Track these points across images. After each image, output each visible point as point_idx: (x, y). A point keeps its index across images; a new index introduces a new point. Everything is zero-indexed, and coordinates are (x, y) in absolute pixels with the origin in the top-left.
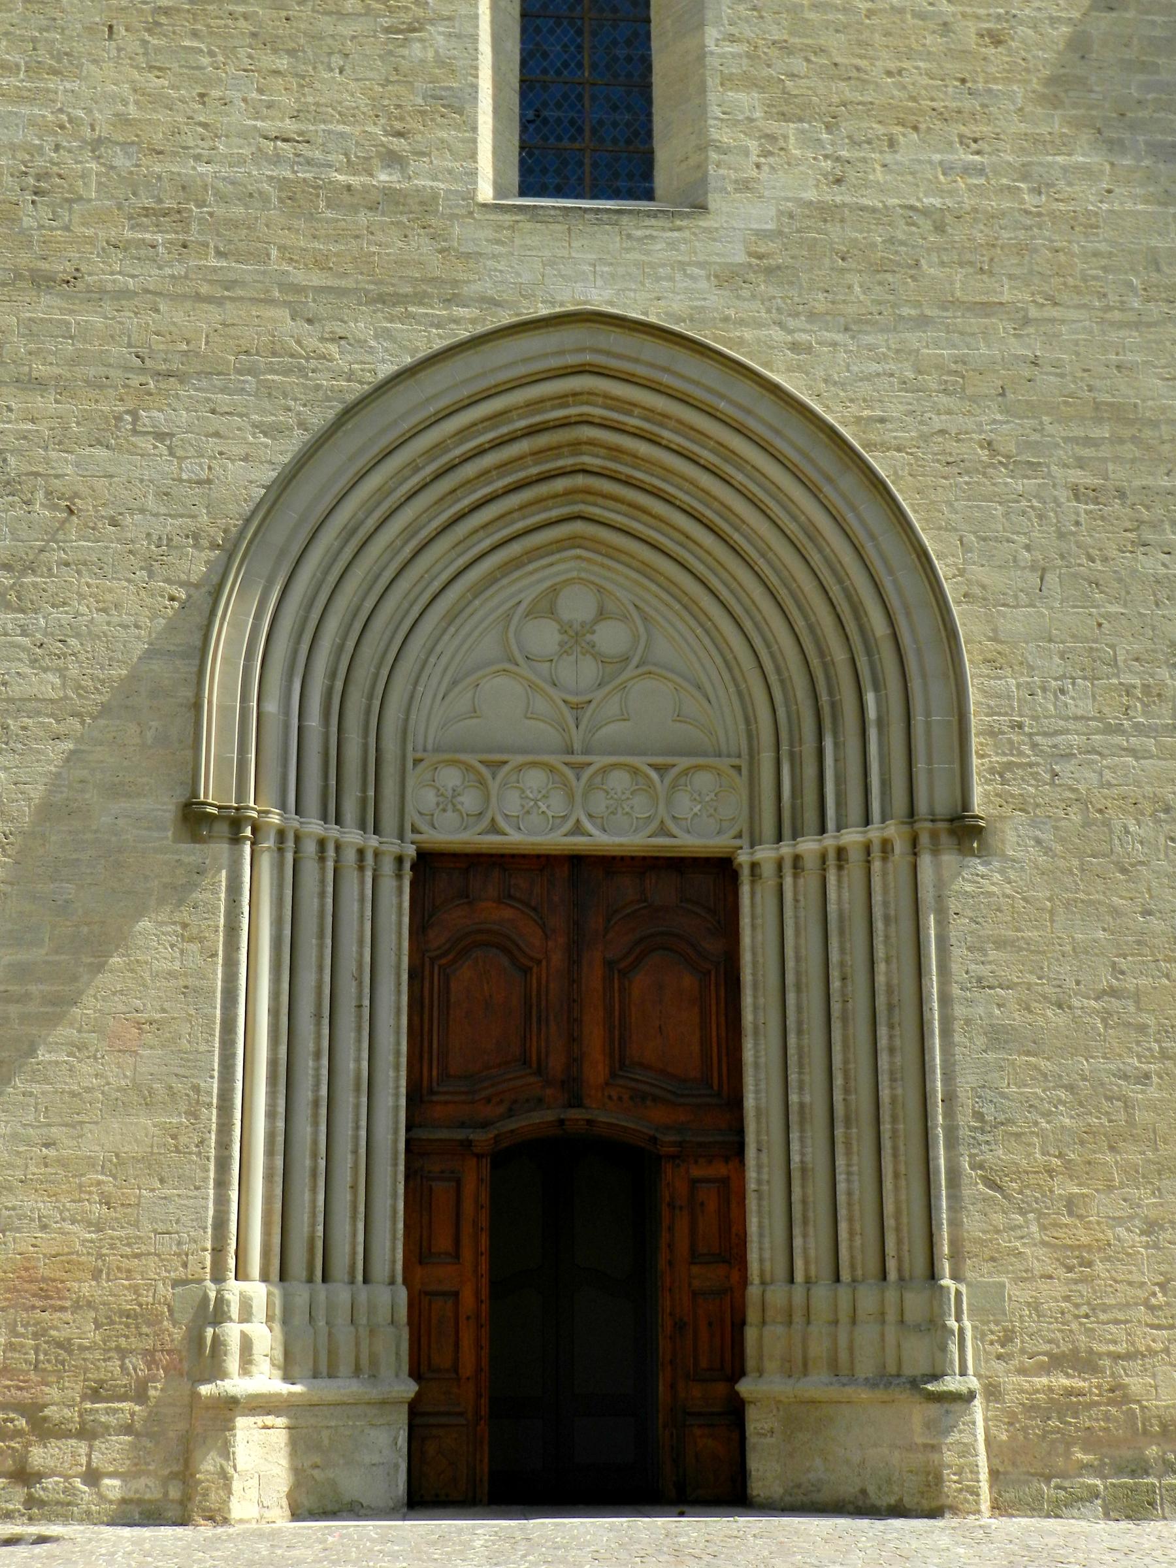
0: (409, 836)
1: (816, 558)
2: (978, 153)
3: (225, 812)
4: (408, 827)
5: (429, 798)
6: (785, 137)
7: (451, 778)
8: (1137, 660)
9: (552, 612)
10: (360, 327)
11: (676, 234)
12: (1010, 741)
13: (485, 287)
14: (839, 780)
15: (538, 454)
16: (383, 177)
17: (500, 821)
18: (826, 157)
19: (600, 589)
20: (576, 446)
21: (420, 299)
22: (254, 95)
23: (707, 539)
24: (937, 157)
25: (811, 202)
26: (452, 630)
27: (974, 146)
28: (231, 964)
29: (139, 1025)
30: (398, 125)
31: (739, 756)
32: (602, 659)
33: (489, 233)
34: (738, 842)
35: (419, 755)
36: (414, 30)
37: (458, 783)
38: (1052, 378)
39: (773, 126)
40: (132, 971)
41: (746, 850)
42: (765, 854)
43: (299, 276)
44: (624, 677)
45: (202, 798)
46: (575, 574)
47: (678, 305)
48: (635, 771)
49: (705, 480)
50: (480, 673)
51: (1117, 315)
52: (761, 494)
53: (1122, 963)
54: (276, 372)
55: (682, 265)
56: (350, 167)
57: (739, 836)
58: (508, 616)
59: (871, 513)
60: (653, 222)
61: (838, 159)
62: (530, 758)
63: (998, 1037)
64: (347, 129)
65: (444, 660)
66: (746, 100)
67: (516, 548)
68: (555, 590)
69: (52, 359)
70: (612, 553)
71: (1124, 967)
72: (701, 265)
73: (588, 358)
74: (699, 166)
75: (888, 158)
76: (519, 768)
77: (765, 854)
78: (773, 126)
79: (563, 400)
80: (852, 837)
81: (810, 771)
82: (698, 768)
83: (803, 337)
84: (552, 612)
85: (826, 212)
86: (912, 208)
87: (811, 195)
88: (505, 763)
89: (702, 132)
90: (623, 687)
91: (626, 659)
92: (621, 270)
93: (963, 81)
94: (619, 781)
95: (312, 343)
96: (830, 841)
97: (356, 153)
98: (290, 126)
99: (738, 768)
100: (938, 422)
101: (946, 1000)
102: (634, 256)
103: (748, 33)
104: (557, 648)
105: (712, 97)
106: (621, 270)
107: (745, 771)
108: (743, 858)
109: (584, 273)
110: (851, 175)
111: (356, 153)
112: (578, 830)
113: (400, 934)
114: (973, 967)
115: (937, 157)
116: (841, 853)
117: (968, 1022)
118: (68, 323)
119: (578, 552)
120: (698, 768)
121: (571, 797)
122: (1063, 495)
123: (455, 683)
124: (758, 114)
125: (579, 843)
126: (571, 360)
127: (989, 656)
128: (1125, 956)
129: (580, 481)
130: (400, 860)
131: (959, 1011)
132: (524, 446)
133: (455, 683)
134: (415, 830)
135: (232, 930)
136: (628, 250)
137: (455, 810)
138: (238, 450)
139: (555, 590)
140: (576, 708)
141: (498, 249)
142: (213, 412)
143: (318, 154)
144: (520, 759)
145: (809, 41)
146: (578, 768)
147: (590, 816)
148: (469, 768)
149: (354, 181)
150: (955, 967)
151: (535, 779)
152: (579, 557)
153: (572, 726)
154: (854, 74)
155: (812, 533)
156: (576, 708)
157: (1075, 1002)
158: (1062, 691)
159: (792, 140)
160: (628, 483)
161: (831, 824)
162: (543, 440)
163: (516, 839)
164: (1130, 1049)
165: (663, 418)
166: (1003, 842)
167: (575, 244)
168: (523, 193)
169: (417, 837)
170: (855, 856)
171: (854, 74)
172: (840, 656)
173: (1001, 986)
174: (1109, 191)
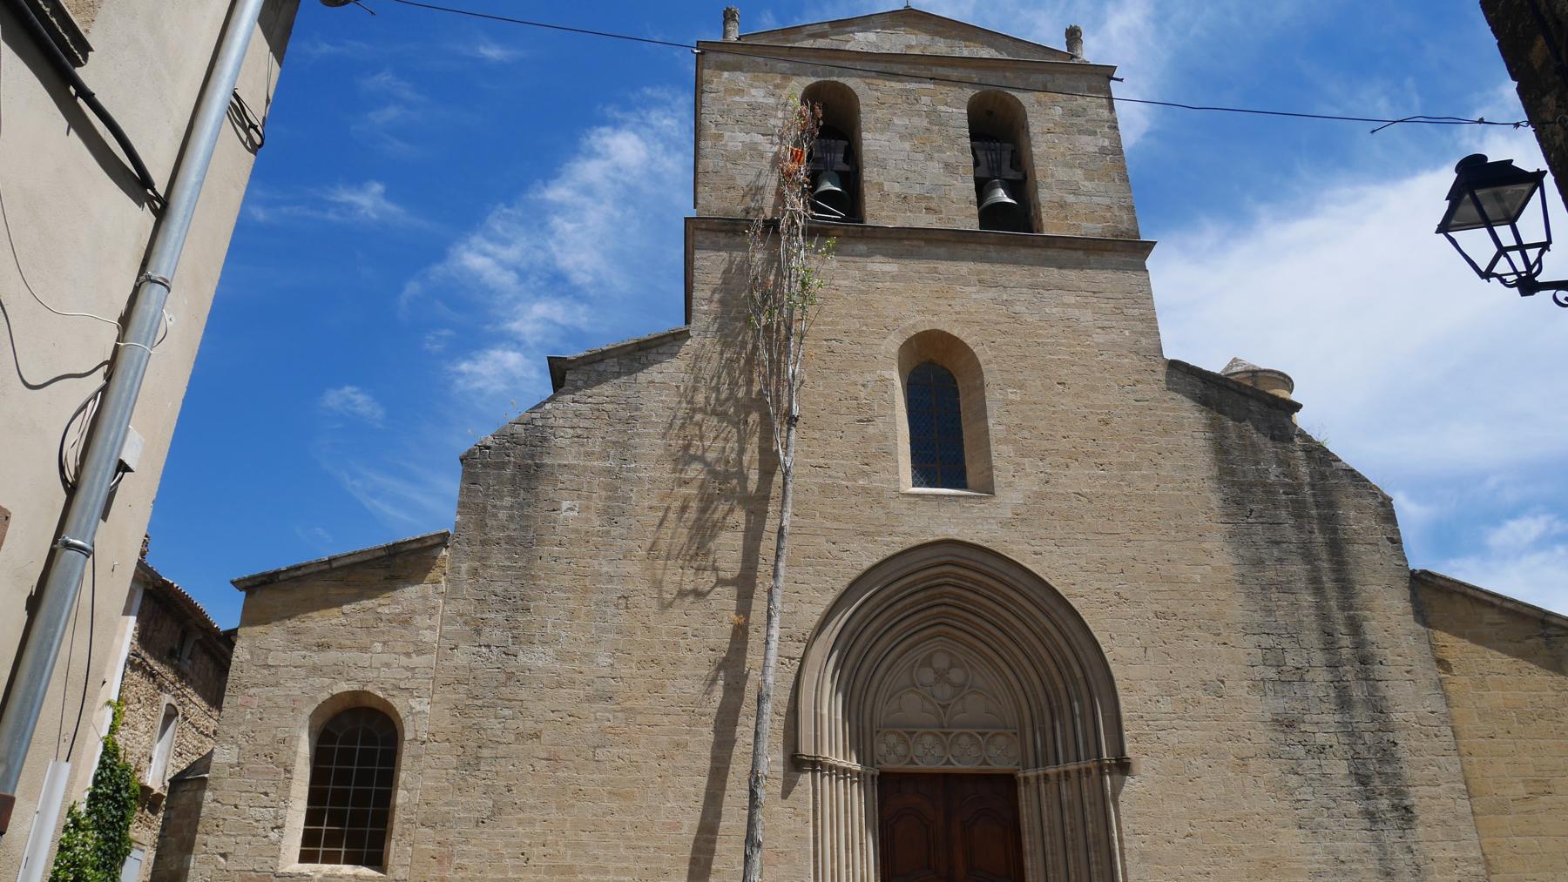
0: (876, 766)
1: (1048, 643)
2: (1103, 470)
3: (810, 759)
4: (875, 762)
5: (884, 748)
6: (1024, 464)
7: (892, 739)
8: (1188, 687)
9: (930, 665)
10: (855, 546)
11: (982, 505)
12: (1139, 724)
13: (906, 529)
14: (1064, 740)
15: (927, 599)
16: (861, 482)
17: (915, 758)
18: (1041, 472)
19: (951, 654)
20: (942, 595)
21: (879, 534)
22: (806, 448)
23: (998, 634)
24: (1087, 472)
25: (1036, 491)
26: (889, 673)
27: (1101, 468)
28: (815, 826)
29: (777, 854)
30: (866, 461)
31: (1015, 728)
32: (952, 685)
33: (905, 506)
34: (1017, 767)
35: (878, 729)
36: (870, 421)
37: (895, 741)
38: (1142, 565)
39: (1018, 460)
40: (774, 829)
41: (1022, 771)
42: (1031, 773)
43: (828, 524)
44: (962, 694)
45: (827, 756)
46: (940, 648)
47: (985, 535)
48: (971, 736)
49: (998, 609)
50: (902, 692)
51: (1165, 538)
52: (1023, 615)
53: (1194, 823)
54: (821, 566)
55: (986, 519)
56: (847, 478)
57: (1018, 764)
58: (912, 666)
59: (1072, 623)
60: (972, 500)
61: (1046, 473)
62: (926, 730)
63: (1144, 856)
64: (845, 462)
65: (886, 686)
66: (1007, 450)
67: (916, 637)
68: (931, 656)
69: (728, 560)
70: (956, 639)
71: (1194, 824)
72: (994, 518)
73: (950, 558)
74: (989, 476)
75: (1067, 473)
76: (921, 735)
77: (1031, 773)
78: (1018, 460)
79: (938, 576)
80: (1072, 767)
81: (1049, 737)
82: (998, 734)
83: (1038, 549)
84: (930, 665)
85: (1043, 496)
86: (1079, 494)
87: (1035, 488)
88: (915, 732)
89: (990, 462)
90: (963, 698)
91: (964, 686)
92: (961, 521)
93: (1094, 440)
94: (964, 740)
95: (835, 553)
96: (1061, 768)
97: (849, 472)
98: (822, 461)
99: (1015, 734)
100: (1097, 585)
101: (1121, 840)
102: (966, 515)
103: (1005, 421)
104: (933, 680)
105: (993, 448)
106: (961, 521)
107: (1018, 735)
108: (1021, 775)
109: (945, 522)
110: (1053, 481)
111: (849, 472)
112: (948, 762)
113: (874, 810)
114: (1130, 825)
115: (1087, 472)
116: (1067, 773)
117: (1130, 849)
118: (734, 545)
119: (942, 638)
120: (998, 734)
121: (944, 748)
122: (1151, 615)
123: (891, 696)
124: (1012, 455)
125: (949, 768)
126: (943, 559)
127: (1126, 686)
128: (1194, 819)
129: (943, 608)
130: (873, 776)
131: (1126, 845)
132: (921, 595)
133: (891, 696)
134: (879, 763)
135: (815, 811)
136: (964, 512)
137: (895, 754)
138: (807, 600)
139: (931, 656)
140: (944, 707)
141: (910, 513)
142: (796, 582)
143: (834, 473)
144: (922, 730)
145: (1030, 424)
146: (947, 734)
147: (953, 756)
148: (899, 735)
149: (849, 484)
150: (1123, 826)
151: (928, 739)
152: (941, 641)
153: (942, 714)
154: (1050, 437)
155: (1046, 631)
156: (944, 707)
157: (1175, 841)
158: (1158, 701)
159: (1027, 465)
160: (963, 609)
161: (1061, 760)
162: (929, 592)
163: (922, 766)
164: (1200, 861)
165: (979, 583)
166: (1139, 768)
167: (942, 510)
168: (914, 486)
169: (879, 766)
170: (1074, 775)
171: (1050, 437)
172: (1061, 686)
173: (1143, 833)
174: (1158, 486)
